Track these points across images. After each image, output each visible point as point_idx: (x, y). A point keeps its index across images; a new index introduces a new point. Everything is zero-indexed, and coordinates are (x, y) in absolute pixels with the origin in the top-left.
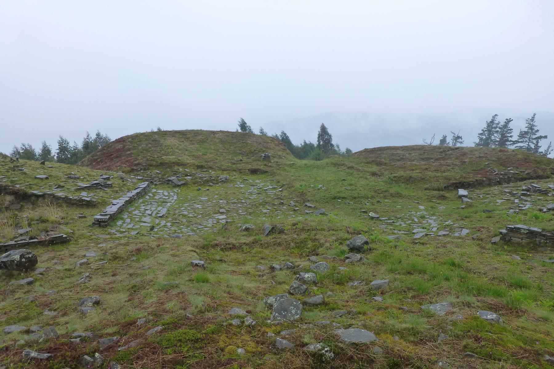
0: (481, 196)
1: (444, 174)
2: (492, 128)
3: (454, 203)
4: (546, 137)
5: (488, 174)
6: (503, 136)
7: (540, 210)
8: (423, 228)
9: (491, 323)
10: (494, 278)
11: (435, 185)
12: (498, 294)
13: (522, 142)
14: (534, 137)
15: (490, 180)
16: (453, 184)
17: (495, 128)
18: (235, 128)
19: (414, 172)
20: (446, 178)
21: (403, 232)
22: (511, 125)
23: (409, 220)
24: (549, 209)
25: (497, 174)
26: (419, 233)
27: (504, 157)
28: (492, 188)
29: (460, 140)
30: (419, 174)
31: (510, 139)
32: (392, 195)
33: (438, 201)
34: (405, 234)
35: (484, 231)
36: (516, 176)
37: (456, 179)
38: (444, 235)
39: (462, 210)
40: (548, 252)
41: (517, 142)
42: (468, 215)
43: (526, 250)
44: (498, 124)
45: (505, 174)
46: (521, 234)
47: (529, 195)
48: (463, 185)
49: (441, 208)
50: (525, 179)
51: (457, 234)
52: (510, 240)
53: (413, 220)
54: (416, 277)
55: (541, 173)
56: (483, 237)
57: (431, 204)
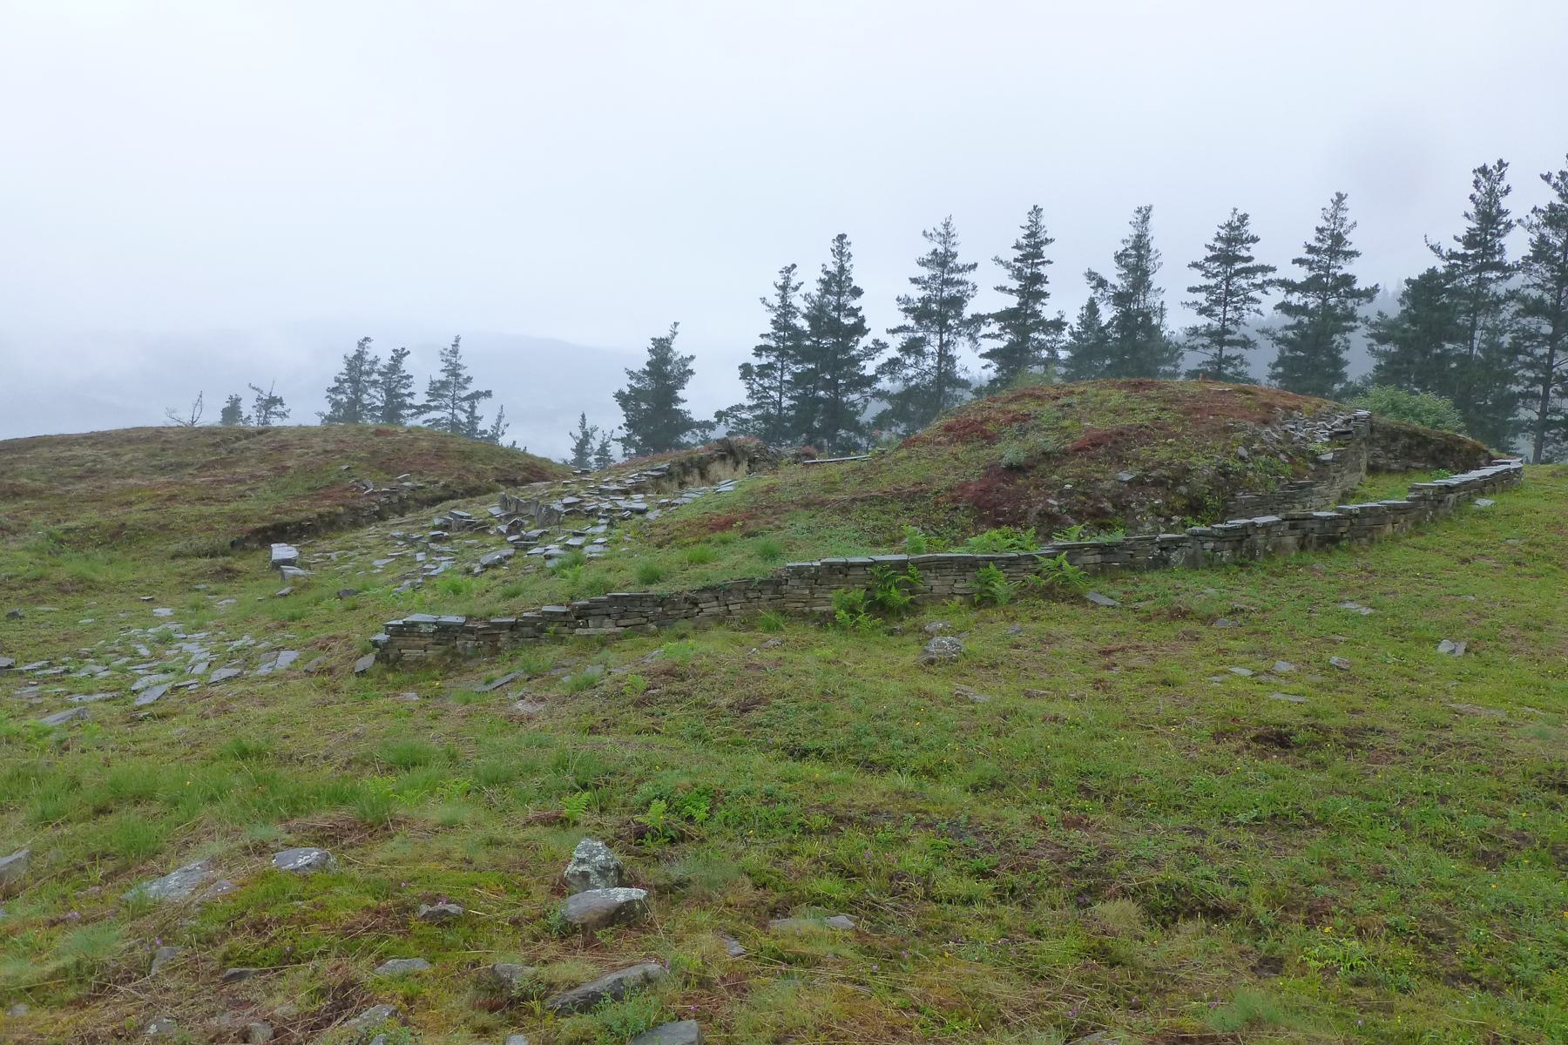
0: (333, 556)
1: (227, 508)
2: (361, 373)
3: (261, 586)
4: (488, 394)
5: (349, 494)
6: (391, 393)
7: (469, 571)
8: (165, 672)
9: (303, 875)
10: (349, 763)
11: (202, 541)
12: (339, 799)
13: (437, 408)
14: (464, 394)
15: (355, 511)
16: (257, 531)
17: (368, 373)
18: (211, 417)
19: (135, 508)
20: (233, 518)
21: (99, 696)
22: (407, 365)
23: (121, 655)
24: (486, 567)
25: (373, 493)
26: (151, 687)
27: (386, 449)
28: (361, 533)
29: (279, 408)
30: (151, 514)
31: (408, 401)
32: (61, 588)
33: (213, 588)
34: (107, 700)
35: (337, 646)
36: (420, 495)
37: (262, 519)
38: (228, 679)
39: (281, 600)
40: (484, 667)
41: (426, 408)
42: (297, 612)
43: (436, 673)
44: (374, 362)
45: (393, 492)
46: (420, 636)
47: (448, 539)
48: (281, 533)
49: (224, 604)
50: (441, 500)
51: (264, 670)
52: (399, 657)
53: (135, 654)
54: (130, 816)
55: (473, 481)
56: (332, 662)
57: (192, 598)
